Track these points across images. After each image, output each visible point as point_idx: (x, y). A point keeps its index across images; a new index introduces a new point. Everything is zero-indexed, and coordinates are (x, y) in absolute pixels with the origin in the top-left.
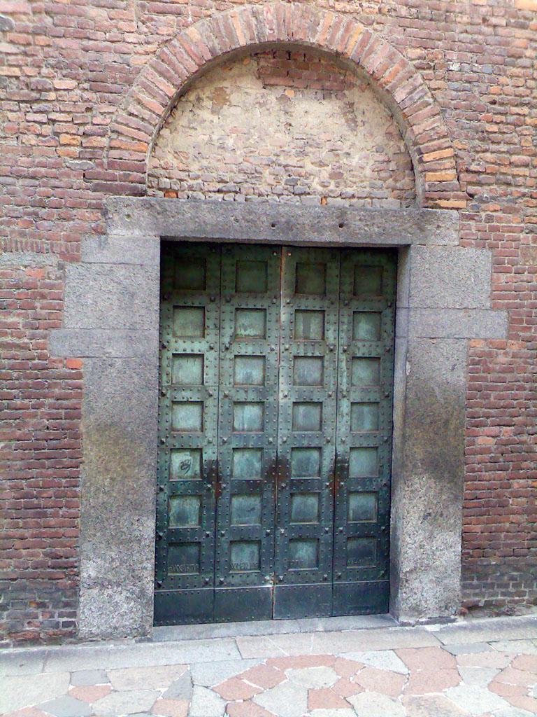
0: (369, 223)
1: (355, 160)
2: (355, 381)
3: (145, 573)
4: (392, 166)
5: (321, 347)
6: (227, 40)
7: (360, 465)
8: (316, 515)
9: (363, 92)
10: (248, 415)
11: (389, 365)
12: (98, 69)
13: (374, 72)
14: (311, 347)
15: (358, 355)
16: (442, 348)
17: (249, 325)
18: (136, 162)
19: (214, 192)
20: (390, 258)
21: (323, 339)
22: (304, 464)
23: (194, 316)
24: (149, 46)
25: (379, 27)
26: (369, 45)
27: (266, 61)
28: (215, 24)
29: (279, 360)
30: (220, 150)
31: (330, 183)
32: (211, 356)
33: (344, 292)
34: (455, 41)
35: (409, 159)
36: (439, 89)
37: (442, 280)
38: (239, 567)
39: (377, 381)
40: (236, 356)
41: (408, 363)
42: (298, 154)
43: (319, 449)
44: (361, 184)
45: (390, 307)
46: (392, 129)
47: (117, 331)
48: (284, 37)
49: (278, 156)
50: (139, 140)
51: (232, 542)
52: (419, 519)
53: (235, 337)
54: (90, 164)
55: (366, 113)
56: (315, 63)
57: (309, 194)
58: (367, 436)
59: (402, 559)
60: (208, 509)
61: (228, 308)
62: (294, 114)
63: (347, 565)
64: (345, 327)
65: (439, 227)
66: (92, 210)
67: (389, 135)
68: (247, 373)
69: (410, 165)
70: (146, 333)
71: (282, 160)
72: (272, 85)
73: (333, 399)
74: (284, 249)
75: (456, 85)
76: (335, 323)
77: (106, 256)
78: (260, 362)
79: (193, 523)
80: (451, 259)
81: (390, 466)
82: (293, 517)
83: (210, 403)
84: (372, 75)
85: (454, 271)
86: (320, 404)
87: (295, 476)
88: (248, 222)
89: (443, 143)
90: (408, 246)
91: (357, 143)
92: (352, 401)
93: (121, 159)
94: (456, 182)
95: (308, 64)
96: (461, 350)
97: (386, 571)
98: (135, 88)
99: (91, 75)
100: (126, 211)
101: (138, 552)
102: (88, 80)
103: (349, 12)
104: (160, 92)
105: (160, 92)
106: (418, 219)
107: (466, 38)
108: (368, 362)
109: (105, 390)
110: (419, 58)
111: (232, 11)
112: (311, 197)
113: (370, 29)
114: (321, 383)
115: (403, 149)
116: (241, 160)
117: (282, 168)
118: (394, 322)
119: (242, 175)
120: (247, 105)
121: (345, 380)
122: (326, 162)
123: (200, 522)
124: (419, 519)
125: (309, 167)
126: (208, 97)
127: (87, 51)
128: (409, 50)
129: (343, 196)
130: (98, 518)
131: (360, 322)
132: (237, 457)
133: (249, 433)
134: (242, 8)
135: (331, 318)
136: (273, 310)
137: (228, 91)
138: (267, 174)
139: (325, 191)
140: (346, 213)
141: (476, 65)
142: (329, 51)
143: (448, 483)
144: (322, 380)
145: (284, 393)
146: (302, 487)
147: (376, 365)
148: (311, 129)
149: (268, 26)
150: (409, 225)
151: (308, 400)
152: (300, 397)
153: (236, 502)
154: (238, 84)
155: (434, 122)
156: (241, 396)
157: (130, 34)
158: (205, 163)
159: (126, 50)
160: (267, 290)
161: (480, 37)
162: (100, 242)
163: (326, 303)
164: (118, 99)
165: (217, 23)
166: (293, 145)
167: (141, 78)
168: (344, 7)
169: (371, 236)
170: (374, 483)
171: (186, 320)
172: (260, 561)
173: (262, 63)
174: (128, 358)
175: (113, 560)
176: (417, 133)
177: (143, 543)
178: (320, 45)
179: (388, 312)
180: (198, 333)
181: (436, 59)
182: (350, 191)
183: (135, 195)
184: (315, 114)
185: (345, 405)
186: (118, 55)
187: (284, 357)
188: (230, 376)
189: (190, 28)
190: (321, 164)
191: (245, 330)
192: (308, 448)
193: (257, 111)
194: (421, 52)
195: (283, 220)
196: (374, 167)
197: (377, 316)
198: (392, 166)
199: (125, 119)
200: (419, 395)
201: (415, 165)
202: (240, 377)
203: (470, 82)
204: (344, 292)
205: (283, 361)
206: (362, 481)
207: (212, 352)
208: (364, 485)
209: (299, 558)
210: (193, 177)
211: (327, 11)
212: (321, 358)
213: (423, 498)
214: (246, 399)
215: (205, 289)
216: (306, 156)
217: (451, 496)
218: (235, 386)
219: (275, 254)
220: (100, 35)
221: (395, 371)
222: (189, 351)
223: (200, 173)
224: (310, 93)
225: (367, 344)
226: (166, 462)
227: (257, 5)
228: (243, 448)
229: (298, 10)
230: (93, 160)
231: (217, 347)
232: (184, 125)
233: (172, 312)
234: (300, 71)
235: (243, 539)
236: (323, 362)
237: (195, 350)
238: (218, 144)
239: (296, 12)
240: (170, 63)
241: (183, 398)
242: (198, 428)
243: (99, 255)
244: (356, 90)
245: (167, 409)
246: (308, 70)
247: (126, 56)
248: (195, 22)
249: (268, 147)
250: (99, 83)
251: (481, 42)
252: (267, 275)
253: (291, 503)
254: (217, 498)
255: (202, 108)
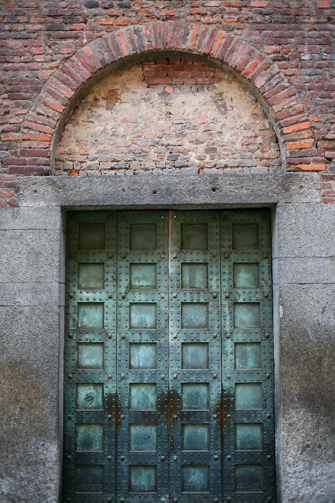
0: (238, 186)
1: (227, 137)
2: (237, 324)
3: (49, 492)
4: (259, 140)
5: (206, 294)
6: (114, 53)
7: (245, 398)
8: (206, 443)
9: (231, 83)
10: (142, 356)
11: (267, 309)
12: (14, 83)
13: (236, 66)
14: (197, 295)
15: (239, 301)
16: (312, 293)
17: (142, 277)
18: (42, 150)
19: (109, 169)
20: (264, 214)
21: (207, 287)
22: (195, 398)
23: (95, 271)
24: (53, 63)
25: (239, 32)
26: (231, 46)
27: (149, 67)
28: (104, 42)
29: (168, 306)
30: (113, 138)
31: (206, 157)
32: (110, 304)
33: (223, 247)
34: (305, 37)
35: (274, 134)
36: (293, 75)
37: (308, 233)
38: (138, 489)
39: (258, 323)
40: (131, 304)
41: (281, 307)
42: (178, 136)
43: (207, 384)
44: (233, 156)
45: (266, 258)
46: (256, 111)
47: (26, 284)
48: (161, 47)
49: (161, 138)
50: (45, 133)
51: (130, 466)
52: (298, 450)
53: (130, 287)
54: (7, 154)
55: (234, 100)
56: (189, 65)
57: (188, 166)
58: (250, 373)
59: (284, 488)
60: (110, 437)
61: (123, 264)
62: (173, 105)
63: (236, 490)
64: (226, 277)
65: (302, 187)
66: (8, 188)
67: (255, 115)
68: (141, 318)
69: (274, 139)
70: (49, 285)
71: (164, 141)
72: (155, 84)
73: (218, 340)
74: (171, 213)
75: (309, 71)
76: (218, 274)
77: (18, 224)
78: (153, 308)
79: (97, 448)
80: (315, 214)
81: (273, 400)
82: (185, 445)
83: (109, 343)
84: (235, 68)
85: (318, 225)
86: (206, 344)
87: (185, 408)
88: (133, 190)
89: (301, 118)
90: (275, 205)
91: (227, 123)
92: (235, 341)
93: (31, 148)
94: (314, 148)
95: (184, 66)
96: (329, 294)
97: (273, 497)
98: (43, 94)
99: (8, 88)
100: (34, 188)
101: (43, 473)
102: (7, 92)
103: (213, 23)
104: (62, 95)
105: (62, 95)
106: (282, 181)
107: (315, 34)
108: (250, 307)
109: (16, 333)
110: (274, 53)
111: (118, 31)
112: (189, 168)
113: (232, 34)
114: (207, 326)
115: (267, 126)
116: (130, 143)
117: (164, 147)
118: (271, 272)
119: (131, 154)
120: (135, 101)
121: (228, 323)
122: (201, 140)
123: (103, 449)
124: (298, 450)
125: (187, 145)
126: (103, 98)
127: (7, 71)
128: (265, 47)
129: (217, 167)
130: (9, 442)
131: (240, 272)
132: (134, 391)
133: (145, 370)
134: (126, 28)
135: (214, 269)
136: (162, 264)
137: (119, 92)
138: (153, 154)
139: (202, 163)
140: (217, 178)
141: (325, 54)
142: (198, 53)
143: (324, 417)
144: (207, 324)
145: (173, 335)
146: (192, 418)
147: (256, 309)
148: (188, 115)
149: (146, 39)
150: (274, 186)
151: (195, 341)
152: (188, 338)
153: (134, 430)
154: (128, 86)
155: (292, 101)
156: (136, 338)
157: (40, 56)
158: (101, 147)
159: (36, 67)
160: (156, 246)
161: (327, 32)
162: (13, 212)
163: (209, 257)
164: (29, 104)
165: (106, 41)
166: (172, 129)
167: (47, 86)
168: (208, 20)
169: (241, 197)
170: (259, 415)
171: (89, 274)
172: (156, 483)
173: (147, 69)
174: (34, 306)
175: (22, 479)
176: (277, 111)
177: (47, 466)
178: (190, 50)
179: (265, 263)
180: (99, 285)
181: (289, 52)
182: (223, 162)
183: (41, 175)
184: (191, 103)
185: (229, 345)
186: (29, 71)
187: (172, 304)
188: (127, 320)
189: (85, 47)
190: (198, 142)
191: (139, 282)
192: (196, 384)
193: (143, 105)
194: (276, 48)
195: (163, 187)
196: (243, 142)
197: (255, 267)
198: (259, 140)
199: (34, 118)
200: (293, 335)
201: (279, 138)
202: (135, 321)
203: (321, 68)
204: (223, 247)
205: (172, 307)
206: (248, 414)
207: (111, 301)
208: (249, 417)
209: (192, 483)
210: (91, 159)
211: (194, 24)
212: (206, 304)
213: (301, 431)
214: (140, 341)
215: (104, 249)
216: (184, 136)
217: (328, 429)
218: (131, 329)
219: (163, 217)
220: (16, 59)
221: (274, 314)
222: (91, 300)
223: (96, 156)
224: (186, 88)
225: (247, 291)
226: (73, 394)
227: (138, 25)
228: (139, 384)
229: (171, 25)
230: (9, 151)
231: (114, 297)
232: (83, 120)
233: (77, 268)
234: (177, 72)
235: (140, 463)
236: (208, 308)
237: (84, 299)
238: (111, 133)
239: (169, 27)
240: (69, 73)
241: (87, 340)
242: (101, 365)
243: (12, 223)
244: (224, 83)
245: (73, 349)
246: (184, 70)
247: (35, 72)
248: (89, 42)
249: (152, 132)
250: (15, 93)
251: (327, 36)
252: (156, 234)
253: (182, 432)
254: (117, 426)
255: (98, 106)
